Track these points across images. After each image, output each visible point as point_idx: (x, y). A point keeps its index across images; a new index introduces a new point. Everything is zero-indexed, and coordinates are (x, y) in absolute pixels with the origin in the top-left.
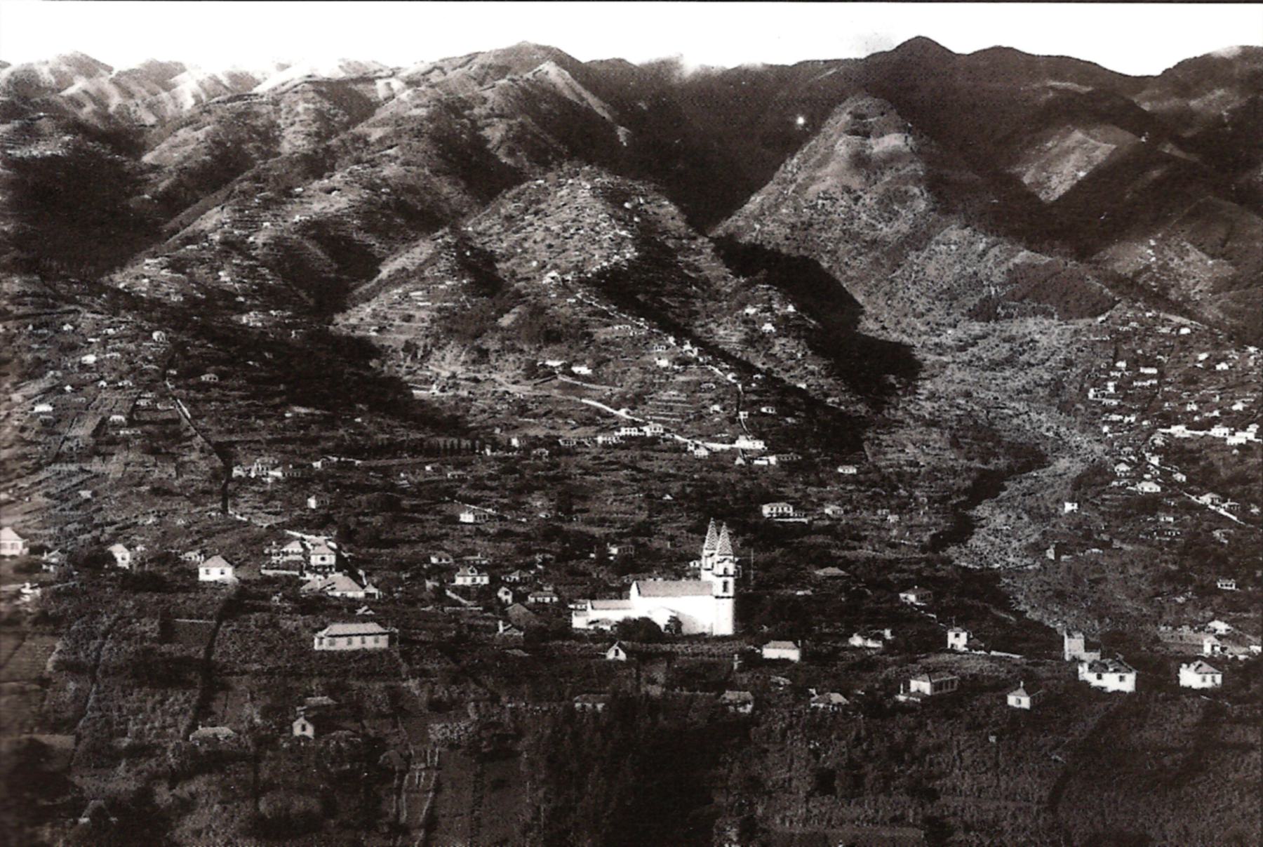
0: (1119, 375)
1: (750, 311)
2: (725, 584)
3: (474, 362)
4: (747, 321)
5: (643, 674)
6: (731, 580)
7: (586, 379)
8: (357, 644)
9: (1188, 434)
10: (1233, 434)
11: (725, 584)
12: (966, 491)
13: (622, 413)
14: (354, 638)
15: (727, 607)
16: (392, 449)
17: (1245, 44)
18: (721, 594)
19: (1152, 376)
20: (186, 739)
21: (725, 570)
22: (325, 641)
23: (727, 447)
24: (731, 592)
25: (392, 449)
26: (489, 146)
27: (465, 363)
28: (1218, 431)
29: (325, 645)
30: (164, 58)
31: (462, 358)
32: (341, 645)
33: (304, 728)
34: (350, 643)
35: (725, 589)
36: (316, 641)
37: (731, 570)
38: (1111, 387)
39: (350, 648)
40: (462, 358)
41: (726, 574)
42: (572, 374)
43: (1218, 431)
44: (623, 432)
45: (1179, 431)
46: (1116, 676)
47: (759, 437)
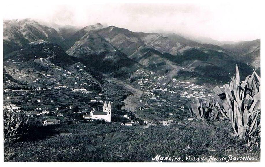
2: (110, 113)
3: (27, 73)
6: (111, 112)
7: (50, 77)
9: (156, 90)
11: (110, 113)
12: (122, 98)
15: (110, 117)
16: (205, 98)
18: (109, 114)
19: (150, 82)
23: (79, 90)
25: (205, 98)
27: (26, 73)
28: (161, 89)
30: (17, 19)
31: (25, 72)
35: (109, 113)
37: (111, 110)
40: (25, 72)
41: (110, 111)
42: (47, 76)
43: (161, 89)
44: (59, 87)
45: (154, 89)
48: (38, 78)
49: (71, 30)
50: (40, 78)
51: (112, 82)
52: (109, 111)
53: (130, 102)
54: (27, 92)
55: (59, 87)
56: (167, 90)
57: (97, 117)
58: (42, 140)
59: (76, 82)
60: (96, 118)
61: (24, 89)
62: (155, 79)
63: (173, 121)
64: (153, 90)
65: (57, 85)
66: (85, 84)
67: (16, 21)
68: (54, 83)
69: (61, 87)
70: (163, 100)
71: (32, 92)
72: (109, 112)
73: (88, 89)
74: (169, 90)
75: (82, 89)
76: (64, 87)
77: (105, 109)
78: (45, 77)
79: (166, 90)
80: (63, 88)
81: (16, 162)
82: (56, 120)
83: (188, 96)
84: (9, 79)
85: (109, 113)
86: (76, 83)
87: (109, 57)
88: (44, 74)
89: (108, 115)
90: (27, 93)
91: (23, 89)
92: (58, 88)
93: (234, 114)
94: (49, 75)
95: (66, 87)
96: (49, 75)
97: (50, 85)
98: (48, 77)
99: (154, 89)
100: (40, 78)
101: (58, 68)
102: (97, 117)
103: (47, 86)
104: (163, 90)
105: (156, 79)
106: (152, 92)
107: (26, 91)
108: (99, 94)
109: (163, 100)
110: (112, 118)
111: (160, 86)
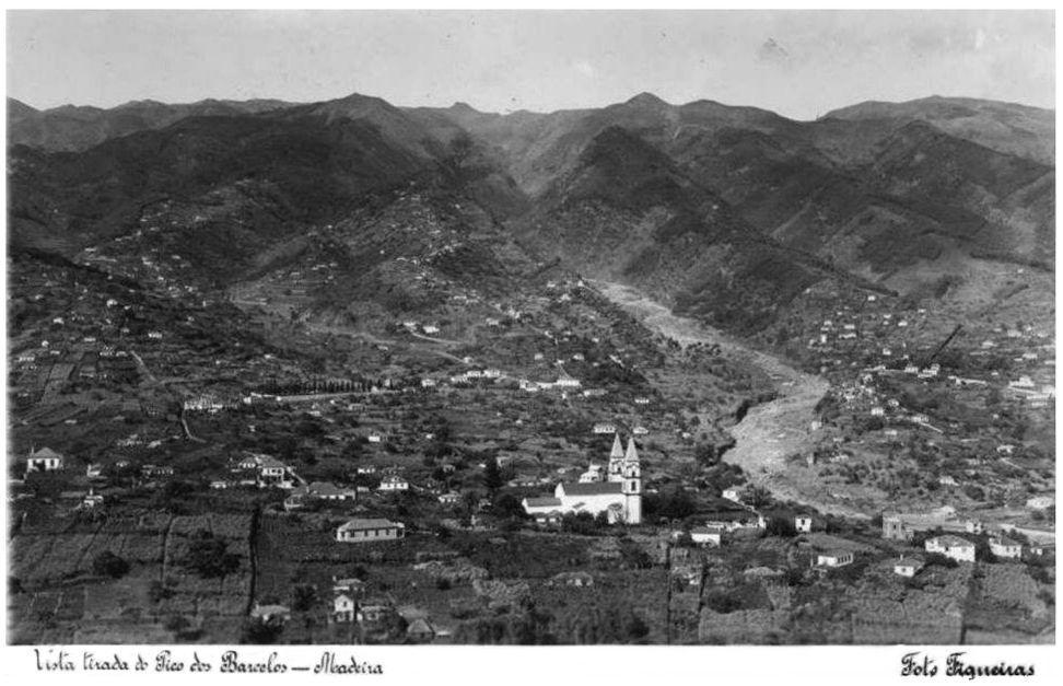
0: (827, 329)
1: (551, 285)
2: (633, 484)
4: (550, 294)
5: (42, 566)
7: (433, 334)
8: (372, 536)
10: (921, 371)
13: (466, 360)
14: (391, 531)
17: (1057, 115)
18: (630, 492)
19: (852, 331)
20: (184, 613)
21: (634, 473)
22: (347, 534)
24: (638, 490)
26: (677, 165)
27: (339, 325)
29: (347, 538)
31: (336, 321)
32: (360, 537)
33: (345, 604)
34: (377, 534)
35: (634, 488)
36: (339, 535)
37: (638, 473)
38: (824, 339)
39: (366, 539)
45: (881, 369)
46: (960, 549)
47: (573, 376)
48: (388, 342)
49: (160, 109)
50: (393, 342)
51: (695, 346)
52: (630, 474)
53: (766, 428)
54: (332, 402)
55: (470, 374)
56: (938, 373)
57: (582, 504)
58: (288, 610)
59: (541, 350)
60: (576, 506)
61: (324, 390)
62: (886, 323)
63: (951, 510)
64: (875, 374)
65: (463, 370)
66: (576, 357)
67: (311, 111)
68: (449, 362)
69: (477, 374)
70: (917, 419)
71: (354, 400)
72: (630, 481)
73: (590, 379)
74: (949, 369)
75: (562, 382)
76: (488, 374)
77: (616, 470)
78: (415, 334)
79: (934, 371)
80: (486, 378)
81: (466, 641)
82: (386, 523)
83: (1036, 395)
84: (266, 353)
85: (634, 488)
86: (539, 356)
87: (686, 238)
88: (410, 325)
89: (628, 495)
90: (335, 408)
91: (320, 388)
92: (464, 378)
93: (328, 660)
94: (430, 329)
95: (497, 373)
96: (430, 329)
97: (433, 370)
98: (423, 337)
99: (881, 369)
100: (393, 342)
101: (469, 297)
102: (582, 504)
103: (420, 371)
104: (921, 371)
105: (891, 321)
106: (869, 384)
107: (328, 400)
108: (637, 401)
109: (917, 419)
110: (648, 506)
111: (906, 357)
